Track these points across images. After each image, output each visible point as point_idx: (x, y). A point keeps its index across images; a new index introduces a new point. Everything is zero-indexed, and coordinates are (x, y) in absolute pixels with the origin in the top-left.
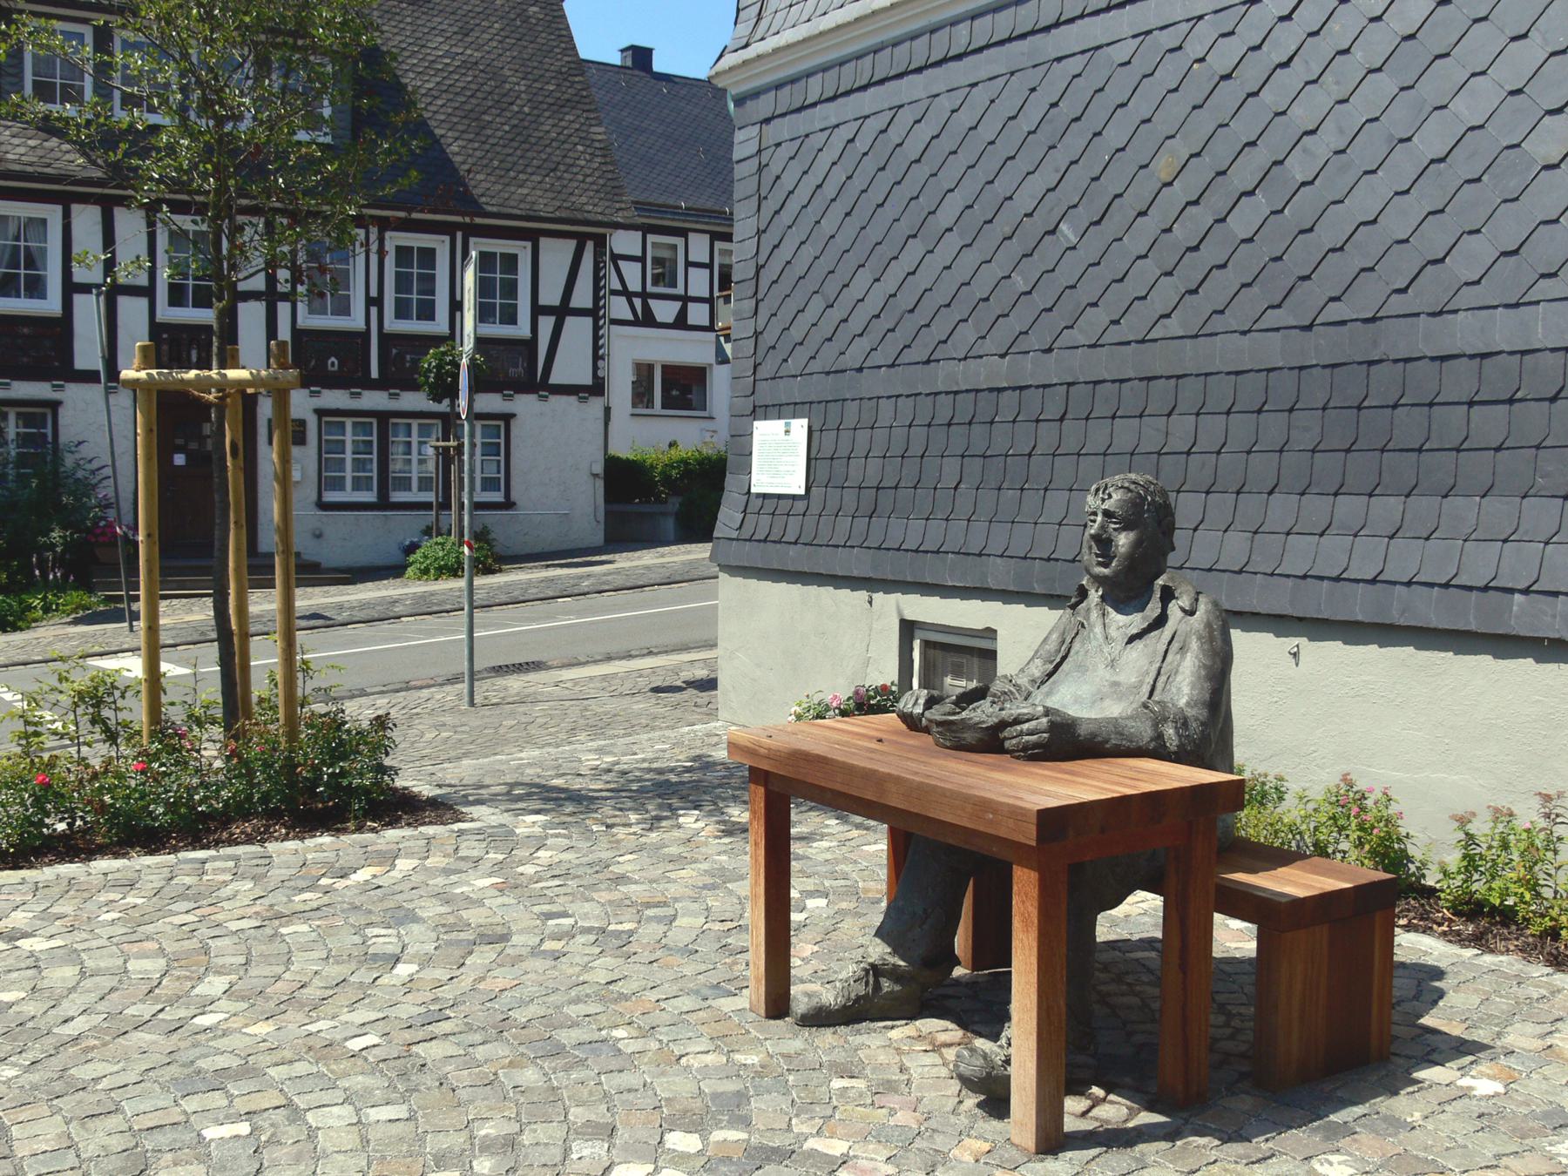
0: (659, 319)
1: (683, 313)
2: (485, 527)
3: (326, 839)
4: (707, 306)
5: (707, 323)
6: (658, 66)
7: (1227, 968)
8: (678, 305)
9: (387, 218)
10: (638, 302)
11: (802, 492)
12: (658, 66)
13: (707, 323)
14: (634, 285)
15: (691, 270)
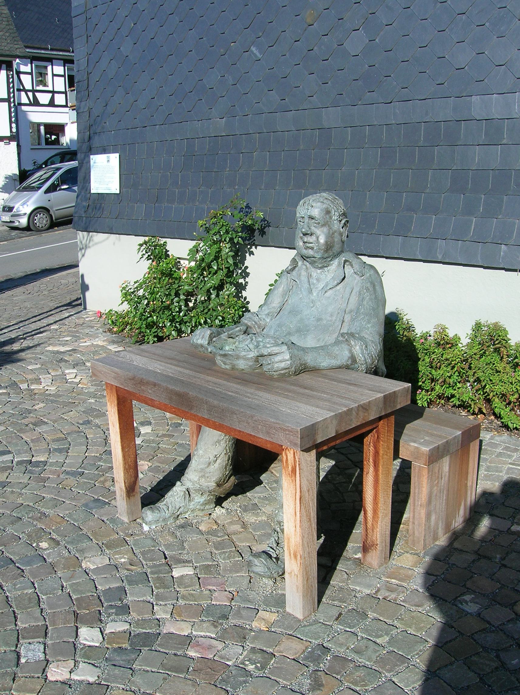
0: (41, 102)
1: (52, 100)
3: (395, 475)
4: (64, 95)
5: (65, 104)
7: (122, 426)
8: (51, 95)
9: (53, 184)
10: (30, 94)
11: (119, 192)
13: (65, 104)
14: (28, 86)
15: (55, 77)
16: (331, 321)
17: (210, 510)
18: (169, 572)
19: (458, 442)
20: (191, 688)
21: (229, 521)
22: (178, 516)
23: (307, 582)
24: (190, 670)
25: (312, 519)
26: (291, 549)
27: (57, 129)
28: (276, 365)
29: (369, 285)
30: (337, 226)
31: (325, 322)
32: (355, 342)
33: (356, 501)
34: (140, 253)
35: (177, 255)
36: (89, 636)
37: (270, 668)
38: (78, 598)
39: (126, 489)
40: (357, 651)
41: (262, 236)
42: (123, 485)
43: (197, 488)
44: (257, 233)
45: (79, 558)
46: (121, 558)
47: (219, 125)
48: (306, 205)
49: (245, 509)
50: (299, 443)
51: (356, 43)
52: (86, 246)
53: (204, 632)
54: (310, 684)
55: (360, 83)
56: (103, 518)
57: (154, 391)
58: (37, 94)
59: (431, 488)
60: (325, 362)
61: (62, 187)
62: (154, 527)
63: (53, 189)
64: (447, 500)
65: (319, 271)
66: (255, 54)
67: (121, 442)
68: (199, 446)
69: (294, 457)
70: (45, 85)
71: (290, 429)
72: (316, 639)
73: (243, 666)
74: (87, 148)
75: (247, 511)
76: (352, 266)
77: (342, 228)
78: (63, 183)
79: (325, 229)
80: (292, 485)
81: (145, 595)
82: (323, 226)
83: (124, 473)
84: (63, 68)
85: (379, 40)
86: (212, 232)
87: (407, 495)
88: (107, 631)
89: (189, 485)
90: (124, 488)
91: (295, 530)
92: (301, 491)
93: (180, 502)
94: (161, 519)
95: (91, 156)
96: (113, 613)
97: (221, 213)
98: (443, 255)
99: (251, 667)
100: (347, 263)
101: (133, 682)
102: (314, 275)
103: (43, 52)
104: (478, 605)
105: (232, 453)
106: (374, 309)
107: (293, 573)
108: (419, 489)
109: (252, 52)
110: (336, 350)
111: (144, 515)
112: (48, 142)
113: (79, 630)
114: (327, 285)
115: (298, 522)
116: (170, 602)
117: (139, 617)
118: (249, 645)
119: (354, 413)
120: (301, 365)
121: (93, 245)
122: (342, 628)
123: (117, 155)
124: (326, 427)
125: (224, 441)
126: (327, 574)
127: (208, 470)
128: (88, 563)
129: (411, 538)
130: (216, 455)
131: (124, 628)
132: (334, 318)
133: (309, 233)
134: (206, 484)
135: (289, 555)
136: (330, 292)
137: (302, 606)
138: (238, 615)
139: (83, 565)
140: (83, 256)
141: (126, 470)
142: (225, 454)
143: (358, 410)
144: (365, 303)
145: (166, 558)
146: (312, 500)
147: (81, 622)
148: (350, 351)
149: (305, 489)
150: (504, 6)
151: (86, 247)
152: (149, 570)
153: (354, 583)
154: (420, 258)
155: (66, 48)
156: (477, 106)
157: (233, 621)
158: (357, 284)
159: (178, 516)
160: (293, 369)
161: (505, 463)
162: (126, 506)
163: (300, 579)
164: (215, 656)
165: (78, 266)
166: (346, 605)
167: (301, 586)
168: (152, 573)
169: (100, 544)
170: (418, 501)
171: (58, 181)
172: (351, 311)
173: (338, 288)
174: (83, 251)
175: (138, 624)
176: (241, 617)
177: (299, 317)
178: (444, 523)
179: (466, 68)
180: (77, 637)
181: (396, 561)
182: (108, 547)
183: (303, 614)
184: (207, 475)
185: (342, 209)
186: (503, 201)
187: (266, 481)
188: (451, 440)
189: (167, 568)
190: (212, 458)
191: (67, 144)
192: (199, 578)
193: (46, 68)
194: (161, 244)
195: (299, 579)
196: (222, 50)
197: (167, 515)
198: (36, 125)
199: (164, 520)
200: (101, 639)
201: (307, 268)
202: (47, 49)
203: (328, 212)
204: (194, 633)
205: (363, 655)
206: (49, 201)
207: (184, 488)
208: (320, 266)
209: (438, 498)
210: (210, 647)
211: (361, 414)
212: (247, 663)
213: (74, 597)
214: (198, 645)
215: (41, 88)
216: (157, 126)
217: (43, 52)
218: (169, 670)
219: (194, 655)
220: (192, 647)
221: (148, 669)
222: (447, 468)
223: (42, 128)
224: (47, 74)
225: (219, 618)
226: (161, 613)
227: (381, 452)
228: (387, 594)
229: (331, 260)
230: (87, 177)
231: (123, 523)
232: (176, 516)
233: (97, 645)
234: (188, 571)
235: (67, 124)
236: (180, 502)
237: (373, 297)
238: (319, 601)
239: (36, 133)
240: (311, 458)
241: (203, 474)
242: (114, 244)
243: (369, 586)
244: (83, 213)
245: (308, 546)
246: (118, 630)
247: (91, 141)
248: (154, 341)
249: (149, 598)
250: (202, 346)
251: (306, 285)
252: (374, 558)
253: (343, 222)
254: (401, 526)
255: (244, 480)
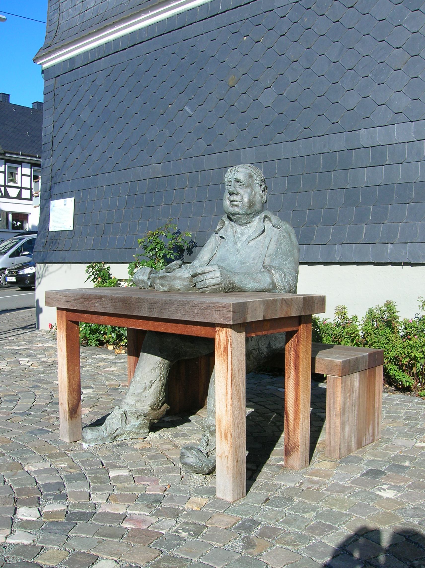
1: (20, 194)
2: (325, 378)
4: (29, 191)
6: (12, 101)
8: (19, 190)
9: (17, 250)
11: (72, 229)
12: (12, 101)
13: (29, 198)
15: (23, 177)
16: (254, 263)
17: (144, 435)
18: (105, 473)
19: (366, 361)
20: (125, 548)
21: (161, 442)
22: (115, 437)
23: (237, 464)
24: (124, 537)
25: (242, 400)
26: (222, 430)
27: (22, 217)
28: (208, 282)
29: (285, 234)
30: (259, 190)
31: (248, 265)
32: (275, 271)
33: (275, 431)
34: (88, 275)
35: (118, 278)
36: (26, 513)
37: (203, 536)
38: (19, 488)
39: (69, 410)
40: (286, 522)
41: (190, 255)
42: (67, 406)
43: (134, 411)
44: (185, 253)
45: (22, 464)
46: (61, 464)
47: (158, 169)
48: (233, 171)
49: (176, 436)
50: (232, 316)
51: (268, 98)
52: (42, 275)
53: (139, 512)
54: (242, 545)
55: (271, 127)
56: (46, 440)
57: (100, 304)
58: (8, 189)
59: (345, 398)
60: (250, 285)
61: (24, 253)
62: (93, 445)
63: (16, 254)
64: (358, 415)
65: (243, 228)
66: (188, 112)
67: (68, 365)
68: (136, 374)
69: (227, 336)
70: (15, 182)
71: (223, 305)
72: (246, 515)
73: (176, 534)
74: (48, 195)
75: (177, 437)
76: (270, 221)
77: (263, 192)
78: (25, 250)
79: (249, 190)
80: (224, 364)
81: (82, 487)
82: (246, 187)
83: (68, 394)
84: (30, 169)
85: (286, 94)
86: (148, 249)
87: (323, 420)
88: (45, 510)
89: (127, 408)
90: (67, 409)
91: (227, 410)
92: (232, 369)
93: (117, 424)
94: (100, 438)
95: (51, 202)
96: (51, 499)
97: (157, 232)
98: (340, 258)
99: (184, 534)
100: (267, 219)
101: (68, 545)
102: (239, 231)
103: (15, 156)
104: (395, 491)
105: (166, 381)
106: (290, 251)
107: (224, 455)
108: (334, 399)
109: (186, 110)
110: (259, 276)
111: (84, 434)
112: (14, 227)
113: (17, 510)
114: (250, 237)
115: (229, 400)
116: (106, 492)
117: (76, 501)
118: (181, 520)
119: (279, 304)
120: (230, 283)
121: (48, 274)
122: (270, 507)
123: (73, 199)
124: (255, 310)
125: (159, 369)
126: (253, 474)
127: (144, 394)
128: (31, 467)
129: (328, 448)
130: (151, 381)
131: (61, 509)
132: (256, 261)
133: (235, 192)
134: (142, 407)
135: (220, 437)
136: (252, 242)
137: (232, 487)
138: (171, 498)
139: (25, 468)
140: (39, 284)
141: (70, 392)
142: (160, 380)
143: (282, 302)
144: (283, 246)
145: (103, 465)
146: (242, 381)
147: (20, 504)
148: (271, 278)
149: (236, 368)
150: (383, 61)
151: (42, 276)
152: (87, 472)
153: (277, 479)
154: (321, 261)
155: (33, 155)
156: (365, 137)
157: (165, 504)
158: (275, 234)
159: (115, 437)
160: (223, 285)
161: (404, 409)
162: (68, 427)
163: (230, 459)
164: (149, 527)
165: (34, 289)
166: (272, 493)
167: (231, 468)
168: (89, 474)
169: (43, 455)
170: (333, 411)
171: (21, 249)
172: (270, 255)
173: (259, 238)
174: (39, 280)
175: (74, 505)
176: (175, 501)
177: (226, 262)
178: (356, 438)
179: (355, 109)
180: (15, 514)
181: (314, 466)
182: (49, 457)
183: (233, 497)
184: (142, 399)
185: (262, 177)
186: (388, 210)
187: (194, 420)
188: (360, 357)
189: (104, 470)
190: (148, 384)
191: (29, 229)
192: (134, 478)
193: (17, 169)
194: (105, 268)
195: (229, 459)
196: (161, 111)
197: (105, 435)
198: (5, 213)
199: (102, 439)
200: (39, 515)
201: (233, 226)
202: (19, 154)
203: (251, 176)
204: (129, 512)
205: (291, 525)
206: (13, 263)
207: (121, 411)
208: (244, 222)
209: (350, 410)
210: (144, 521)
211: (284, 307)
212: (180, 531)
213: (15, 488)
214: (132, 519)
215: (11, 184)
216: (107, 174)
217: (15, 156)
218: (104, 536)
219: (129, 526)
220: (126, 521)
221: (83, 535)
222: (358, 384)
223: (10, 216)
224: (17, 174)
225: (153, 502)
226: (96, 498)
227: (301, 355)
228: (310, 486)
229: (253, 217)
230: (47, 218)
231: (64, 443)
232: (113, 437)
233: (35, 519)
234: (125, 473)
235: (30, 213)
236: (117, 424)
237: (289, 242)
238: (247, 491)
239: (5, 221)
240: (241, 339)
241: (139, 398)
242: (66, 272)
243: (292, 481)
244: (41, 248)
245: (238, 427)
246: (55, 509)
247: (52, 190)
248: (96, 344)
249: (86, 490)
250: (143, 281)
251: (232, 239)
252: (297, 459)
253: (263, 186)
254: (317, 445)
255: (175, 419)
